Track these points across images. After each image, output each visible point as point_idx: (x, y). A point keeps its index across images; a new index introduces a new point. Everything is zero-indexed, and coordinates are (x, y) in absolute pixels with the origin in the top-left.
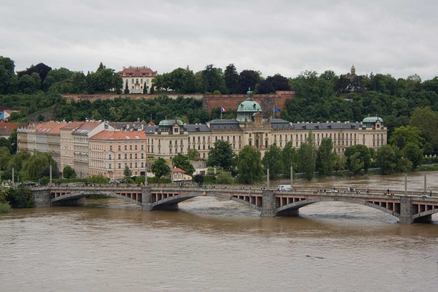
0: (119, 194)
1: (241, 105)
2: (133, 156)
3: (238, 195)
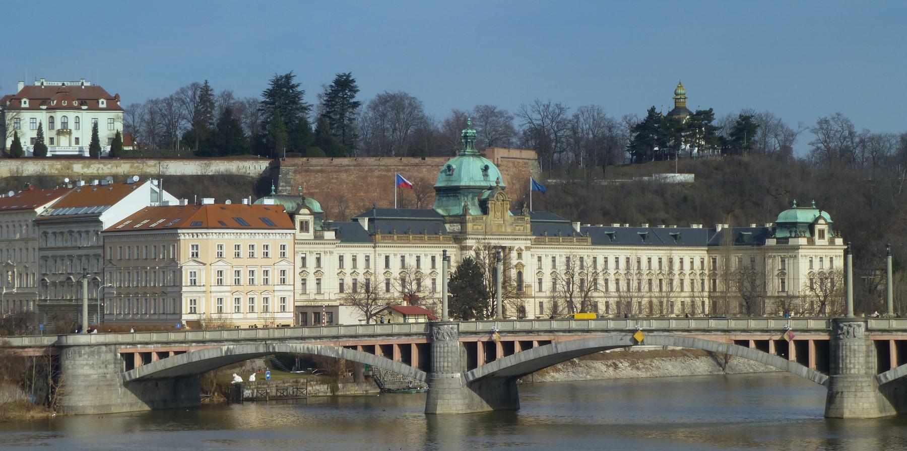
0: (355, 348)
2: (259, 278)
3: (752, 338)
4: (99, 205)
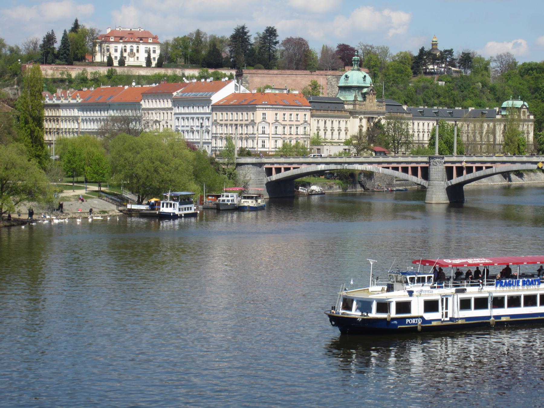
1: (347, 77)
3: (400, 166)
4: (209, 92)
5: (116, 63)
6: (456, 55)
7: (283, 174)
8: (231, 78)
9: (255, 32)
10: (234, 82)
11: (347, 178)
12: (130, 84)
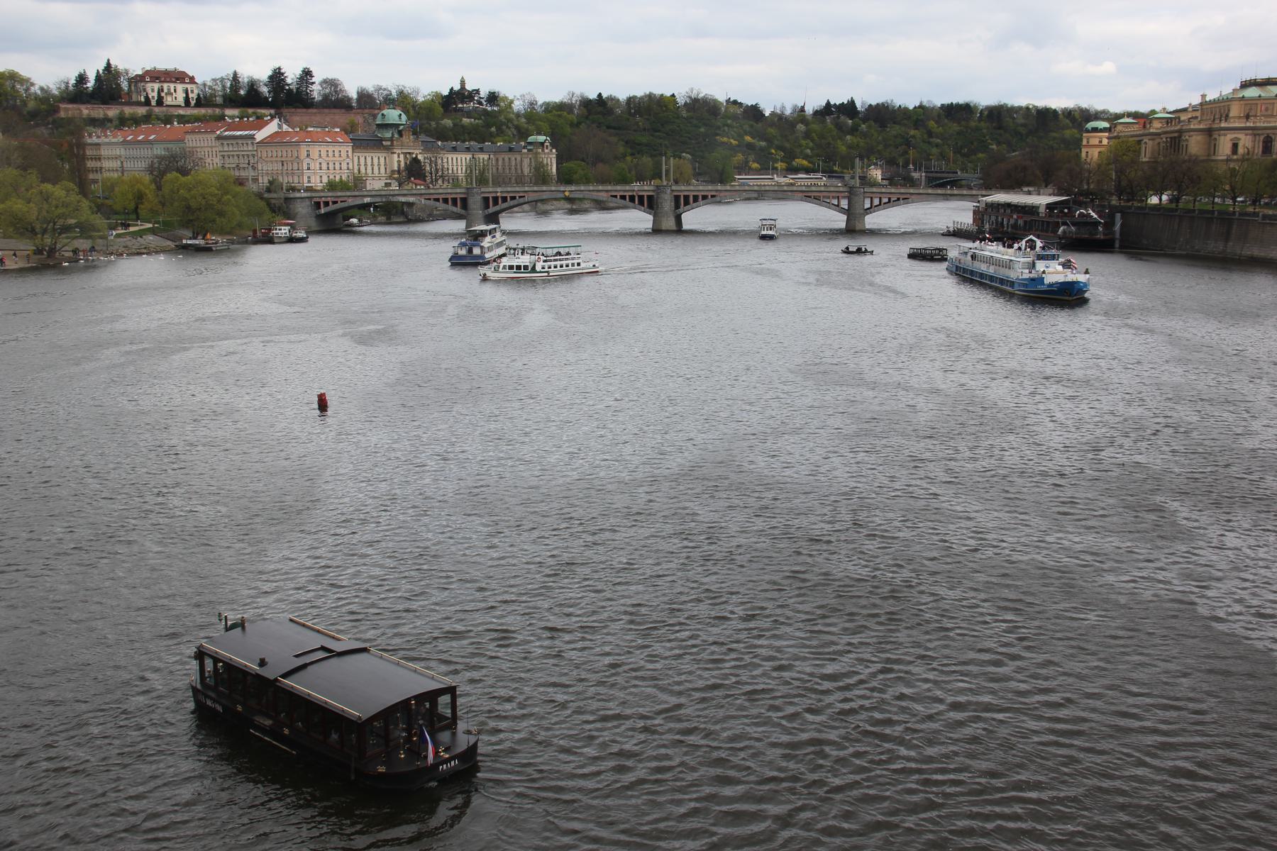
3: (619, 194)
5: (153, 103)
6: (484, 93)
7: (332, 207)
8: (273, 117)
9: (292, 75)
10: (276, 121)
11: (346, 212)
12: (171, 123)
